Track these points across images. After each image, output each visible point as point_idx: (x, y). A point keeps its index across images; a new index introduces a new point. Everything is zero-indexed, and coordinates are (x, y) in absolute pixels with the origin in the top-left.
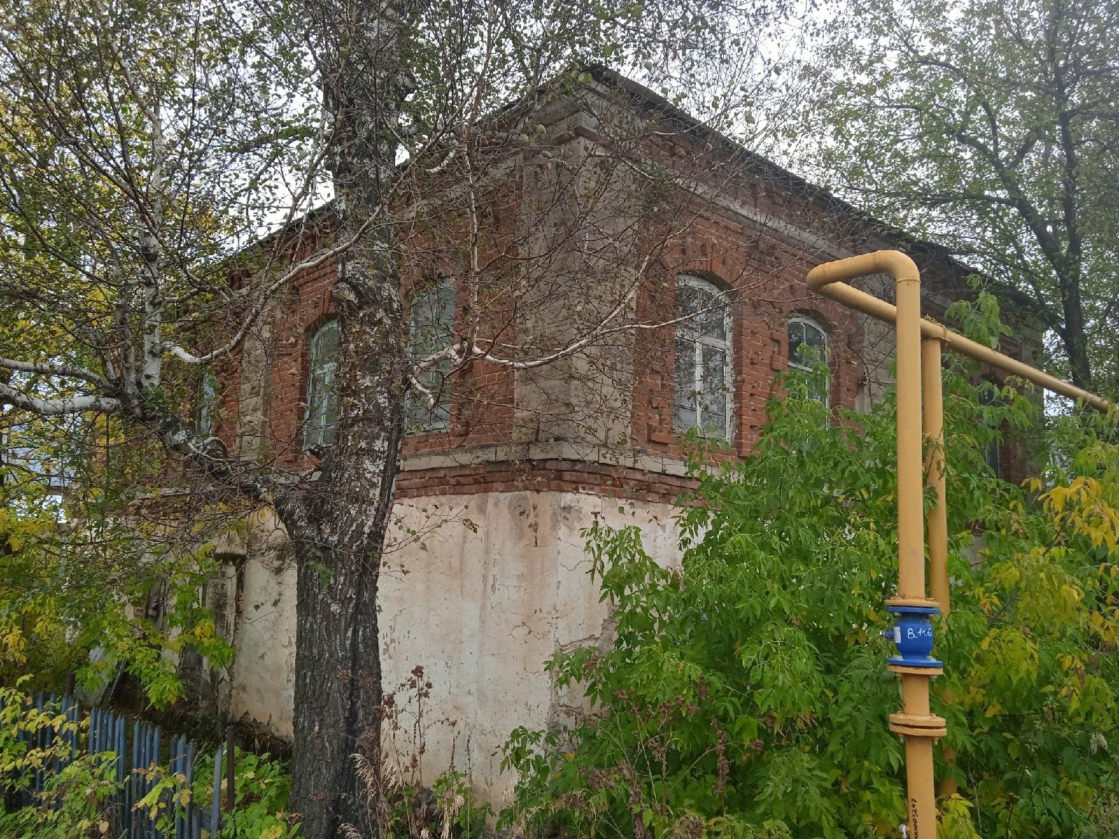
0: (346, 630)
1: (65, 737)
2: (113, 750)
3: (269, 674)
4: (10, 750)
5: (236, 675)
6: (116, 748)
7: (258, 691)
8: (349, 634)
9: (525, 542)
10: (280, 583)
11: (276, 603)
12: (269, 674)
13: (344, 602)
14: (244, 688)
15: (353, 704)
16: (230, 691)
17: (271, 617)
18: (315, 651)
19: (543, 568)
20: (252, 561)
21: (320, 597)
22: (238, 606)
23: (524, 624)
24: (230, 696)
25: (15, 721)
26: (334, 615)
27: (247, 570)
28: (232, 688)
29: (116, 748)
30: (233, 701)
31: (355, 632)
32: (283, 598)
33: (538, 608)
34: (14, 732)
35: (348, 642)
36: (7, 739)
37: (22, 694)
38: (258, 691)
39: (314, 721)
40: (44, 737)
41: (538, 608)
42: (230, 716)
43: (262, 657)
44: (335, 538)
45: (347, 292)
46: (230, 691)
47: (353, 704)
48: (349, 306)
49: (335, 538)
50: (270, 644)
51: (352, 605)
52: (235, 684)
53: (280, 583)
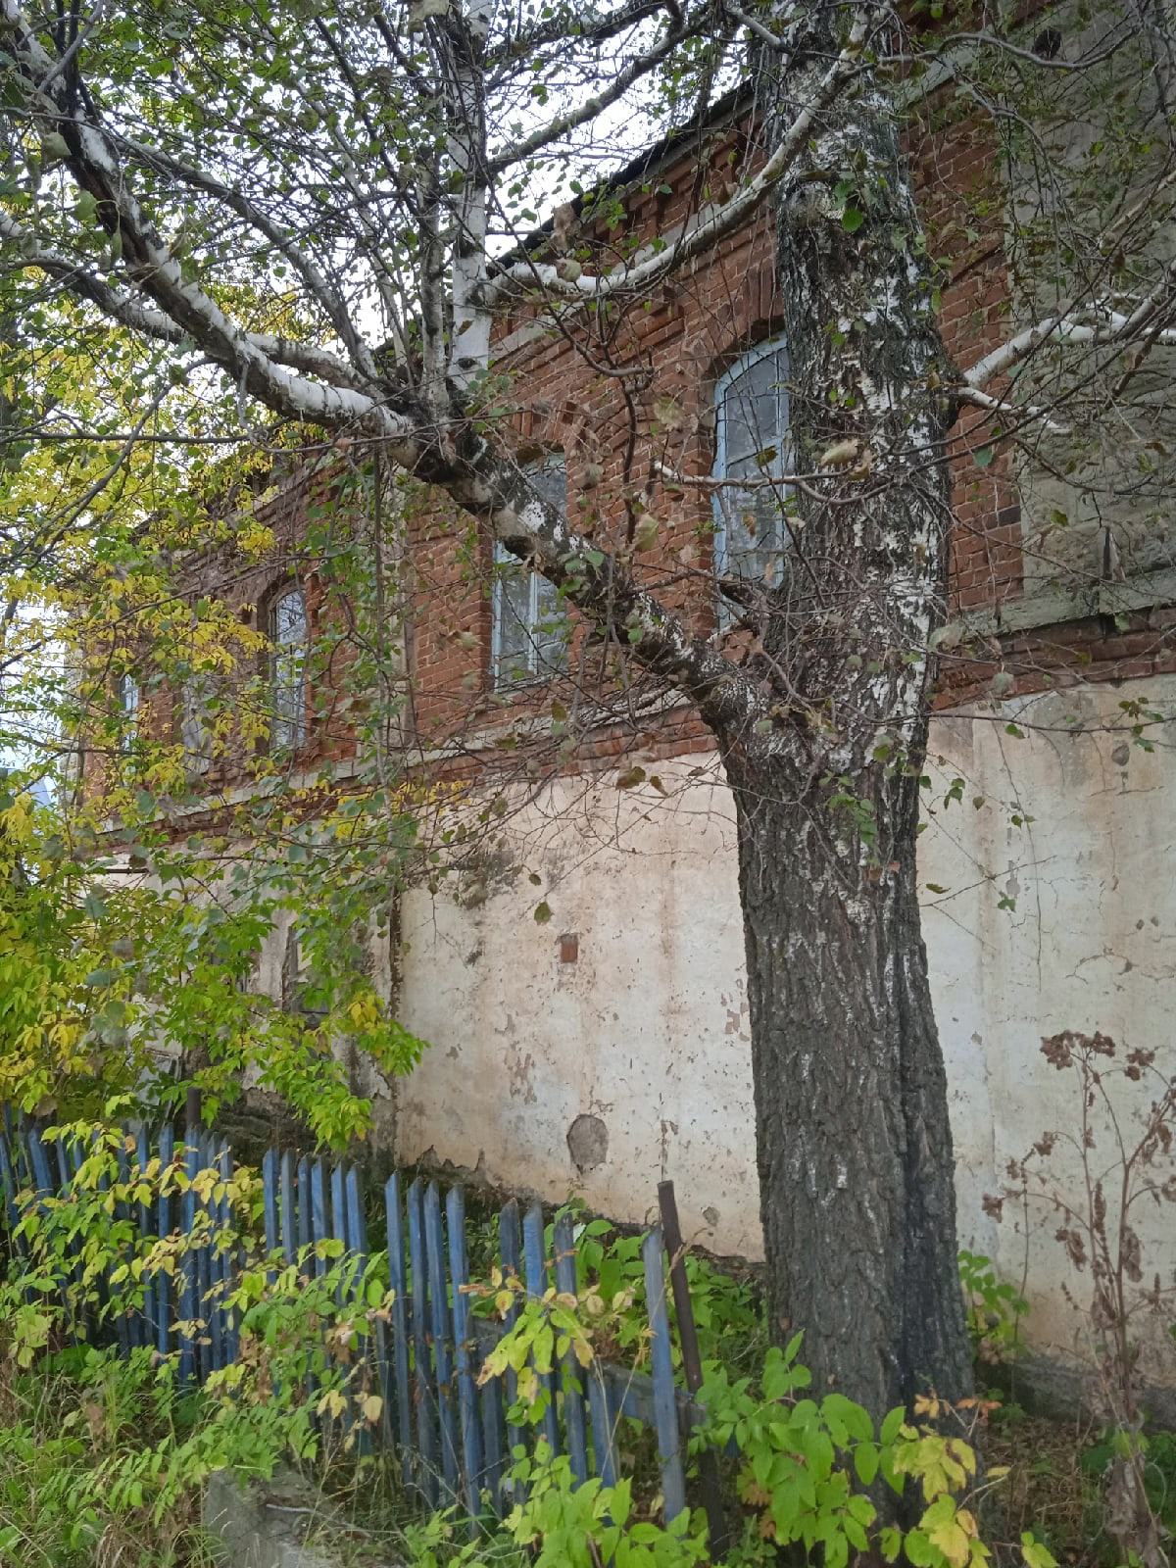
0: (882, 959)
1: (217, 1212)
2: (330, 1234)
3: (470, 1083)
4: (102, 1240)
5: (401, 1087)
6: (338, 1229)
7: (451, 1112)
8: (889, 966)
9: (1088, 789)
10: (478, 924)
11: (473, 959)
12: (470, 1083)
13: (875, 892)
14: (420, 1110)
15: (910, 1122)
16: (393, 1116)
17: (466, 984)
18: (819, 1007)
19: (1151, 833)
20: (415, 892)
21: (818, 888)
22: (394, 970)
23: (1107, 952)
24: (395, 1123)
25: (107, 1182)
26: (856, 927)
27: (404, 908)
28: (396, 1109)
29: (338, 1229)
30: (399, 1130)
31: (898, 962)
32: (487, 949)
33: (1146, 917)
34: (109, 1205)
35: (889, 985)
36: (95, 1218)
37: (118, 1131)
38: (451, 1112)
39: (832, 1162)
40: (172, 1212)
41: (1146, 917)
42: (396, 1158)
43: (453, 1053)
44: (845, 755)
45: (825, 201)
46: (393, 1116)
47: (910, 1122)
48: (832, 233)
49: (845, 755)
50: (469, 1028)
51: (889, 902)
52: (400, 1102)
53: (478, 924)
